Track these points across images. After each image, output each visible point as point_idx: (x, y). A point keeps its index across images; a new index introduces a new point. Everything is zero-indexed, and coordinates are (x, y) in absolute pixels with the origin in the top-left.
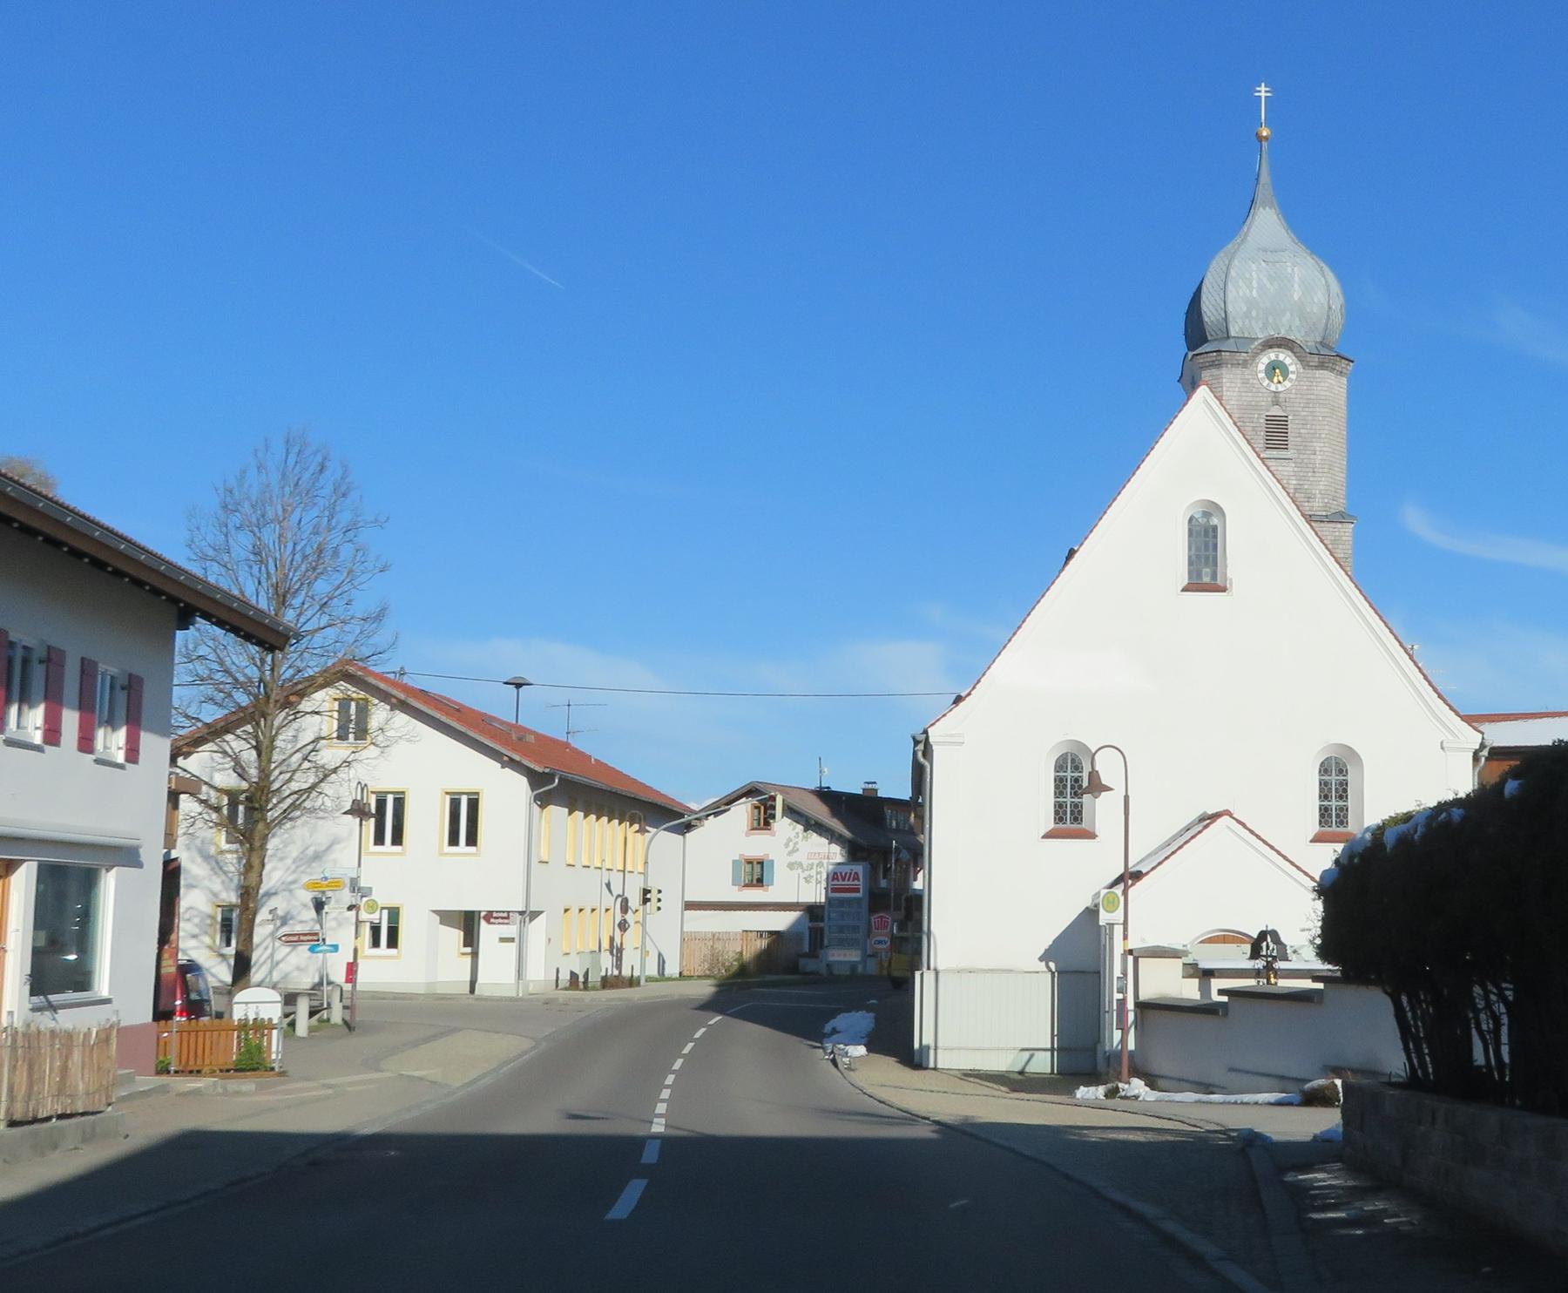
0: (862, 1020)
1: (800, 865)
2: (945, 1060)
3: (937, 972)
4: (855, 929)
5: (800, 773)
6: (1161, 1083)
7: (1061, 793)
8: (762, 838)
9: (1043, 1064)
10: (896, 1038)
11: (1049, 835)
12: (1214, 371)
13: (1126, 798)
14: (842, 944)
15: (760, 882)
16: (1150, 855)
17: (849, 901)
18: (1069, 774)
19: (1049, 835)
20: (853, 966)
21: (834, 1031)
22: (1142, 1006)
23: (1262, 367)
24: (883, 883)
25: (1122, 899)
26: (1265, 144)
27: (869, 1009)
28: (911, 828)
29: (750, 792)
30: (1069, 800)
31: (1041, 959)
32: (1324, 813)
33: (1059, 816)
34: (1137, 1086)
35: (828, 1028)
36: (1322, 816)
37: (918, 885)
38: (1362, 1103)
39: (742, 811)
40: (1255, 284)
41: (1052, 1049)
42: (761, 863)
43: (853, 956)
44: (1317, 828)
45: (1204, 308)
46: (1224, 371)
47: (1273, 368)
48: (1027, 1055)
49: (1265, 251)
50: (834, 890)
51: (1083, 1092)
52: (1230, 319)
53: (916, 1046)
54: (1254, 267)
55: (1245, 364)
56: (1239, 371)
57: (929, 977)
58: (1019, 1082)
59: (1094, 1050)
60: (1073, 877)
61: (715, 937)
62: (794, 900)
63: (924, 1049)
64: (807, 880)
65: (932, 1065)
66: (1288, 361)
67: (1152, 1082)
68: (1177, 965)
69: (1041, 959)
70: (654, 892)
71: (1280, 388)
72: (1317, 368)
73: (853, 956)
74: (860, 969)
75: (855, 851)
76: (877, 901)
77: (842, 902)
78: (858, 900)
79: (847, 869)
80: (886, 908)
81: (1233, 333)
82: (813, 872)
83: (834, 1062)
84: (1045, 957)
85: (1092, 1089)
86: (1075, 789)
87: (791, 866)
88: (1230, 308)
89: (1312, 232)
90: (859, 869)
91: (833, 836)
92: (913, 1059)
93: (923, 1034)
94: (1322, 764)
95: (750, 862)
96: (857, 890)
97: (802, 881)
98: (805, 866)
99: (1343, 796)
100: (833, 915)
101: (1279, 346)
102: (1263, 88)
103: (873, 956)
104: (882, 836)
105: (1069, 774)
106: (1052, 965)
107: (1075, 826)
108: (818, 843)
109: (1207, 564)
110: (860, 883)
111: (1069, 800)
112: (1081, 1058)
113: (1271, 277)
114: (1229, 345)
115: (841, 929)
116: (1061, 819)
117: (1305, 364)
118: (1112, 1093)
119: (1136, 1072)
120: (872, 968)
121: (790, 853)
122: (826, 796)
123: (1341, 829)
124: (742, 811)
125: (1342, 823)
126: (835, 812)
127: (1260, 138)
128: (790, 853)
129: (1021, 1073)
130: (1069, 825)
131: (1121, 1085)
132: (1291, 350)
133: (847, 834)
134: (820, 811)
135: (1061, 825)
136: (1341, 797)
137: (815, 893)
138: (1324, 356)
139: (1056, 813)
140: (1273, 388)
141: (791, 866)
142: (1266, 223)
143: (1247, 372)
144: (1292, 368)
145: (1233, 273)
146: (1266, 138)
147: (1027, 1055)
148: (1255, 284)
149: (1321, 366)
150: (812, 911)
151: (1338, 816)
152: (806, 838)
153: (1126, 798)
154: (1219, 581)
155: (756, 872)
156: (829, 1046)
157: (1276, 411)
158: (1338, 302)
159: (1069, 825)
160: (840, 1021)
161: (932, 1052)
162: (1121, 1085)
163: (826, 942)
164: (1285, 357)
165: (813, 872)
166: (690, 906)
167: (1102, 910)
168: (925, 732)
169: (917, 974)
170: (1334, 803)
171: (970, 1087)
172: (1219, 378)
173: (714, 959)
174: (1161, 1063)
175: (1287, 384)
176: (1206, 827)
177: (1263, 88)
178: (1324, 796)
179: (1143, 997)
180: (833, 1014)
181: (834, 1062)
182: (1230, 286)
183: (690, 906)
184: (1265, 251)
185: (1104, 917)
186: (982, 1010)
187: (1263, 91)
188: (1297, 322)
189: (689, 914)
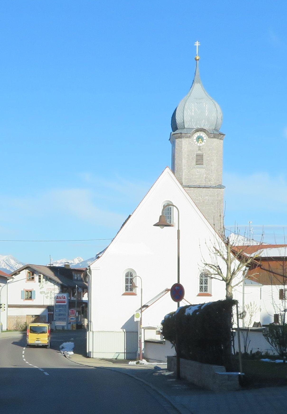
0: (71, 344)
1: (44, 292)
2: (95, 355)
3: (93, 332)
4: (64, 315)
5: (42, 260)
6: (150, 360)
7: (127, 283)
8: (31, 283)
9: (122, 357)
10: (81, 349)
11: (124, 294)
12: (180, 140)
13: (142, 289)
14: (60, 319)
15: (31, 298)
16: (151, 300)
17: (62, 306)
18: (129, 278)
19: (124, 294)
20: (63, 327)
21: (63, 348)
22: (146, 342)
23: (195, 138)
24: (72, 298)
25: (140, 314)
26: (198, 62)
27: (72, 341)
28: (82, 279)
29: (27, 268)
30: (129, 285)
31: (121, 328)
32: (201, 288)
33: (127, 288)
34: (144, 361)
35: (61, 347)
36: (200, 289)
37: (85, 298)
38: (170, 360)
39: (25, 273)
40: (193, 111)
41: (125, 353)
42: (31, 292)
43: (64, 324)
44: (199, 292)
45: (177, 118)
46: (183, 139)
47: (199, 138)
48: (117, 354)
49: (197, 99)
50: (57, 302)
51: (130, 363)
52: (185, 122)
53: (88, 352)
54: (193, 105)
55: (189, 137)
56: (187, 139)
57: (91, 333)
58: (116, 361)
59: (136, 352)
60: (128, 307)
61: (17, 317)
62: (42, 304)
63: (90, 353)
64: (47, 297)
65: (92, 357)
66: (203, 136)
67: (148, 360)
68: (155, 331)
69: (121, 328)
70: (3, 305)
71: (201, 145)
72: (213, 138)
73: (64, 324)
74: (66, 328)
75: (63, 289)
76: (71, 304)
77: (60, 306)
78: (65, 305)
79: (61, 295)
80: (74, 307)
81: (186, 127)
82: (49, 295)
83: (65, 356)
84: (123, 328)
85: (133, 362)
86: (130, 285)
87: (41, 293)
88: (185, 119)
89: (213, 92)
90: (65, 295)
91: (57, 284)
92: (86, 355)
93: (89, 348)
94: (201, 275)
95: (27, 291)
96: (65, 302)
97: (45, 298)
98: (48, 293)
99: (206, 283)
100: (57, 310)
101: (201, 131)
102: (197, 43)
103: (70, 323)
104: (72, 281)
105: (129, 278)
106: (125, 330)
107: (131, 292)
108: (50, 285)
109: (168, 219)
110: (66, 300)
111: (129, 285)
112: (132, 354)
113: (199, 107)
114: (184, 131)
115: (60, 315)
116: (127, 290)
117: (210, 137)
118: (138, 363)
119: (144, 358)
120: (70, 328)
121: (41, 289)
122: (53, 269)
123: (206, 292)
124: (25, 273)
125: (206, 291)
126: (56, 275)
127: (196, 60)
128: (41, 289)
129: (116, 359)
130: (129, 292)
131: (140, 361)
132: (205, 132)
133: (60, 282)
134: (51, 274)
135: (127, 292)
136: (206, 283)
137: (51, 302)
138: (216, 134)
139: (126, 288)
140: (198, 145)
141: (41, 293)
142: (198, 88)
143: (190, 139)
144: (205, 138)
145: (186, 107)
146: (198, 60)
147: (117, 354)
148: (193, 111)
149: (214, 137)
150: (49, 308)
151: (205, 289)
152: (46, 283)
153: (142, 289)
154: (172, 223)
155: (29, 295)
156: (62, 352)
157: (199, 152)
158: (220, 116)
159: (129, 292)
160: (64, 344)
161: (92, 353)
162: (140, 361)
163: (55, 319)
164: (203, 134)
165: (49, 295)
166: (10, 306)
167: (135, 318)
168: (89, 266)
169: (88, 333)
170: (204, 285)
171: (102, 362)
172: (181, 142)
173: (18, 324)
174: (149, 356)
175: (203, 143)
176: (166, 293)
177: (197, 43)
178: (201, 283)
179: (145, 340)
180: (61, 343)
181: (65, 356)
182: (185, 111)
183: (10, 306)
184: (197, 99)
185: (136, 319)
186: (105, 344)
187: (197, 44)
188: (207, 123)
189: (10, 309)
